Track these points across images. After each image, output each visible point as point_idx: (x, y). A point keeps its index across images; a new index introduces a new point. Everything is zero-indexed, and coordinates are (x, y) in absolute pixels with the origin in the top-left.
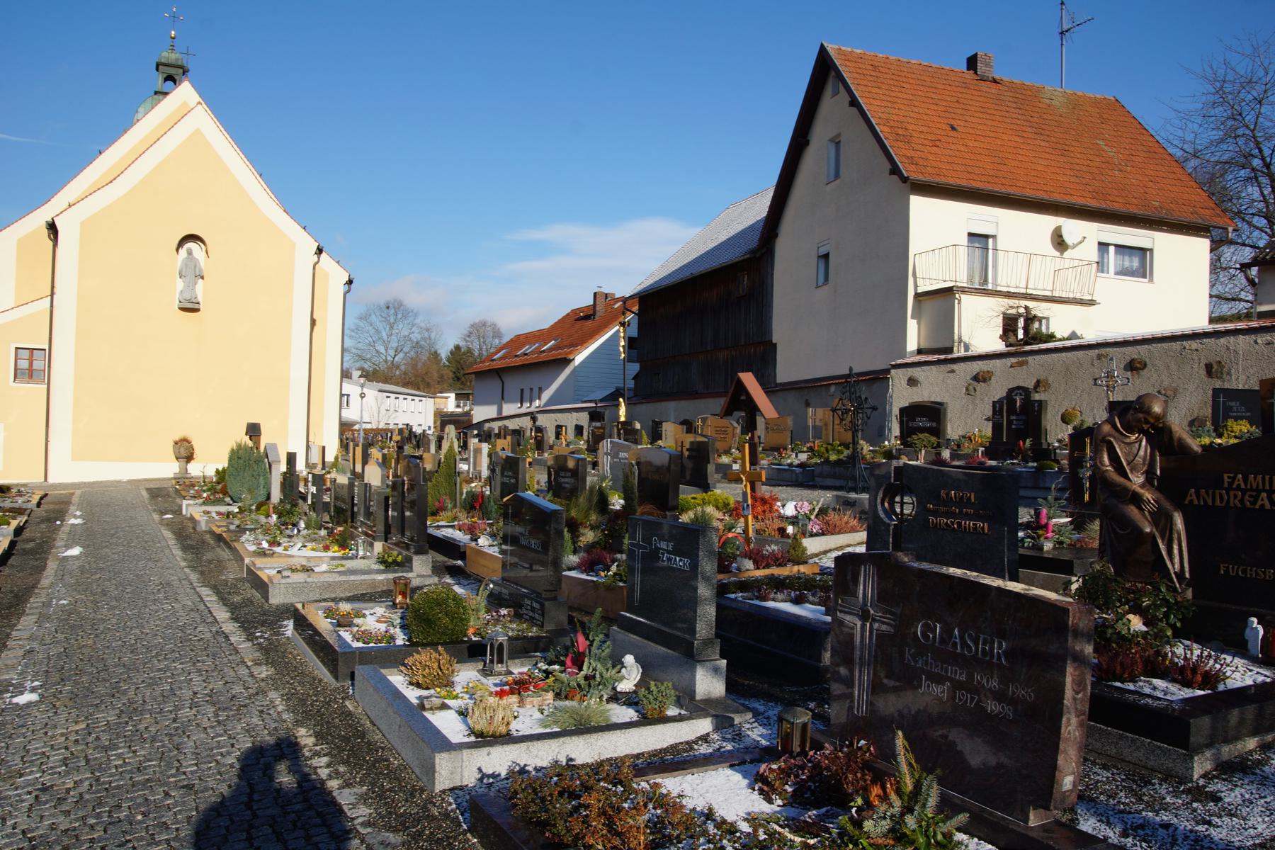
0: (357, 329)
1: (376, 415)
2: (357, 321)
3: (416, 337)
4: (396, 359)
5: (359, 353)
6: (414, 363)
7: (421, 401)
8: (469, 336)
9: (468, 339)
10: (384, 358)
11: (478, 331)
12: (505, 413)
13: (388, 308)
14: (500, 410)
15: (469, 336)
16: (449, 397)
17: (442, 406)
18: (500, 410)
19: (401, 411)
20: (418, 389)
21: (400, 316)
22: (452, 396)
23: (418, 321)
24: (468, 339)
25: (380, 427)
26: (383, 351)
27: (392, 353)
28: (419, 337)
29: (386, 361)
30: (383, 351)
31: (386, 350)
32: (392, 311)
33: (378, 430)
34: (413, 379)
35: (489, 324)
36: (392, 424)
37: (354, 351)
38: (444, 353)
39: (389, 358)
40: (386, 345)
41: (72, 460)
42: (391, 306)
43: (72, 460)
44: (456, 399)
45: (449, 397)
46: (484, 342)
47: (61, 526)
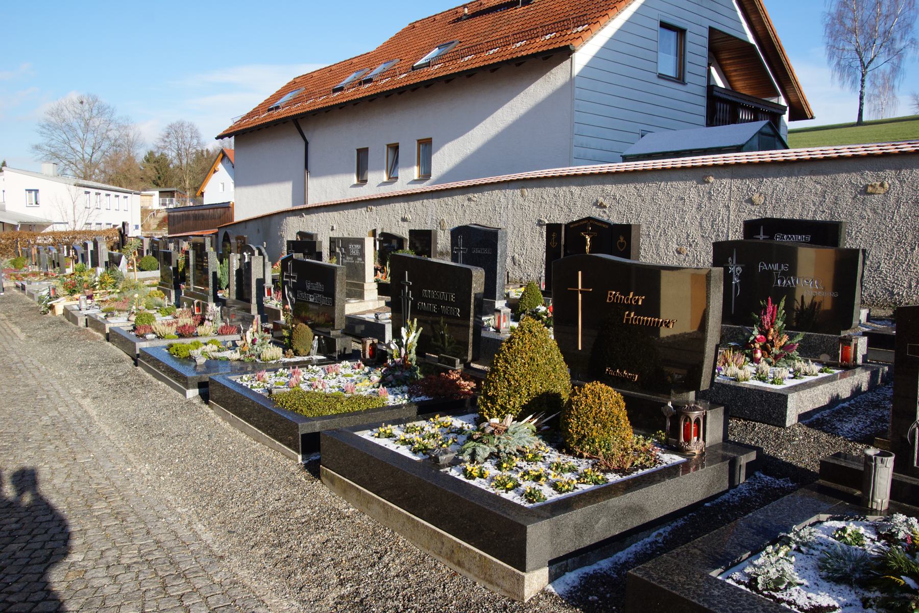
0: (49, 125)
1: (70, 212)
2: (48, 117)
3: (113, 134)
4: (95, 156)
5: (53, 150)
6: (113, 162)
7: (126, 197)
8: (167, 137)
9: (166, 139)
10: (81, 156)
11: (176, 131)
12: (313, 200)
13: (82, 103)
14: (301, 192)
15: (167, 137)
16: (154, 195)
17: (146, 204)
18: (301, 192)
19: (103, 209)
20: (120, 186)
21: (95, 112)
22: (157, 193)
23: (115, 117)
24: (166, 139)
25: (77, 229)
26: (79, 148)
27: (89, 150)
28: (117, 134)
29: (83, 160)
30: (79, 148)
31: (83, 148)
32: (86, 107)
33: (74, 232)
34: (114, 176)
35: (186, 125)
36: (94, 224)
37: (46, 148)
38: (140, 154)
39: (86, 156)
40: (83, 142)
41: (431, 139)
42: (85, 101)
43: (431, 139)
44: (160, 196)
45: (154, 195)
46: (183, 143)
47: (659, 555)
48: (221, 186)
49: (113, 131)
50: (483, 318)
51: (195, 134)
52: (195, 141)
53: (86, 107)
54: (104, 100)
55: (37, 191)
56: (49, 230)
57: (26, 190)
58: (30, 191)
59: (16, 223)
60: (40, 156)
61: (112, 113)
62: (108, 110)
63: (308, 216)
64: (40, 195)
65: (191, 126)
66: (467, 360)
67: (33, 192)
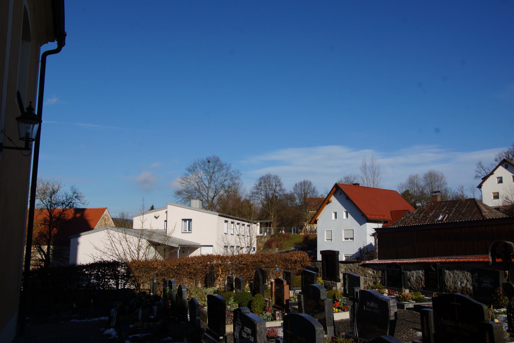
10: (206, 198)
13: (209, 162)
39: (210, 199)
42: (211, 161)
48: (333, 215)
49: (228, 180)
50: (394, 319)
51: (279, 183)
52: (278, 188)
53: (211, 165)
54: (223, 160)
55: (190, 220)
56: (196, 253)
57: (183, 220)
58: (185, 220)
59: (177, 246)
60: (180, 199)
61: (228, 169)
62: (225, 167)
63: (219, 253)
64: (193, 223)
65: (276, 177)
66: (148, 294)
67: (188, 221)
